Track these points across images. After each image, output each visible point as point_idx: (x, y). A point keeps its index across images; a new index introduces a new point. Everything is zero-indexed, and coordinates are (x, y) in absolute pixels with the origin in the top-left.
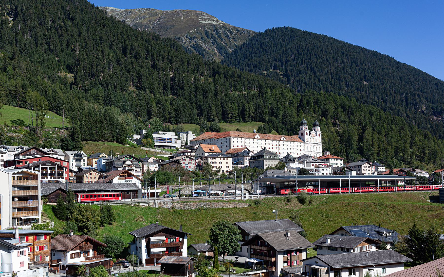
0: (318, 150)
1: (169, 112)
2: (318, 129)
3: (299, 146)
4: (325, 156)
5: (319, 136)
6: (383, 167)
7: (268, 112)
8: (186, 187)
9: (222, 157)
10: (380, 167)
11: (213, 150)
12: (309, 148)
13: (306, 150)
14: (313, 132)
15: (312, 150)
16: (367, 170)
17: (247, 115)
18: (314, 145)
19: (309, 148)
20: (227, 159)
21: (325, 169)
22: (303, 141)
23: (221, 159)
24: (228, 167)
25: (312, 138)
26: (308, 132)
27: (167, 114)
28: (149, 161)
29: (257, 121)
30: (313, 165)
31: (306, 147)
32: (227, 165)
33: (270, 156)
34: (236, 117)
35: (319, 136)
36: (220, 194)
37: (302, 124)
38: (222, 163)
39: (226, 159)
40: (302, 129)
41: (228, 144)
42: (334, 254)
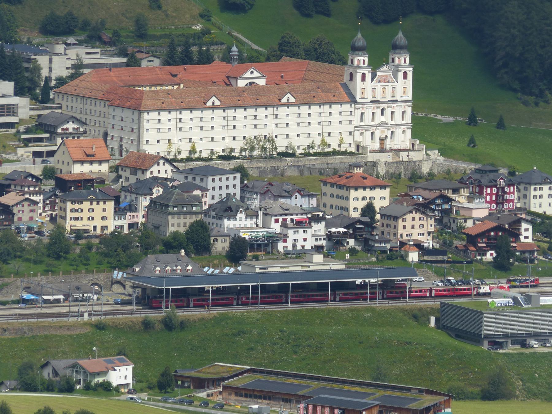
0: (398, 119)
8: (14, 281)
9: (94, 200)
11: (93, 156)
13: (358, 122)
15: (380, 119)
20: (105, 203)
22: (353, 100)
23: (91, 204)
24: (106, 218)
25: (379, 86)
30: (277, 221)
32: (104, 214)
36: (62, 300)
38: (93, 210)
41: (136, 127)
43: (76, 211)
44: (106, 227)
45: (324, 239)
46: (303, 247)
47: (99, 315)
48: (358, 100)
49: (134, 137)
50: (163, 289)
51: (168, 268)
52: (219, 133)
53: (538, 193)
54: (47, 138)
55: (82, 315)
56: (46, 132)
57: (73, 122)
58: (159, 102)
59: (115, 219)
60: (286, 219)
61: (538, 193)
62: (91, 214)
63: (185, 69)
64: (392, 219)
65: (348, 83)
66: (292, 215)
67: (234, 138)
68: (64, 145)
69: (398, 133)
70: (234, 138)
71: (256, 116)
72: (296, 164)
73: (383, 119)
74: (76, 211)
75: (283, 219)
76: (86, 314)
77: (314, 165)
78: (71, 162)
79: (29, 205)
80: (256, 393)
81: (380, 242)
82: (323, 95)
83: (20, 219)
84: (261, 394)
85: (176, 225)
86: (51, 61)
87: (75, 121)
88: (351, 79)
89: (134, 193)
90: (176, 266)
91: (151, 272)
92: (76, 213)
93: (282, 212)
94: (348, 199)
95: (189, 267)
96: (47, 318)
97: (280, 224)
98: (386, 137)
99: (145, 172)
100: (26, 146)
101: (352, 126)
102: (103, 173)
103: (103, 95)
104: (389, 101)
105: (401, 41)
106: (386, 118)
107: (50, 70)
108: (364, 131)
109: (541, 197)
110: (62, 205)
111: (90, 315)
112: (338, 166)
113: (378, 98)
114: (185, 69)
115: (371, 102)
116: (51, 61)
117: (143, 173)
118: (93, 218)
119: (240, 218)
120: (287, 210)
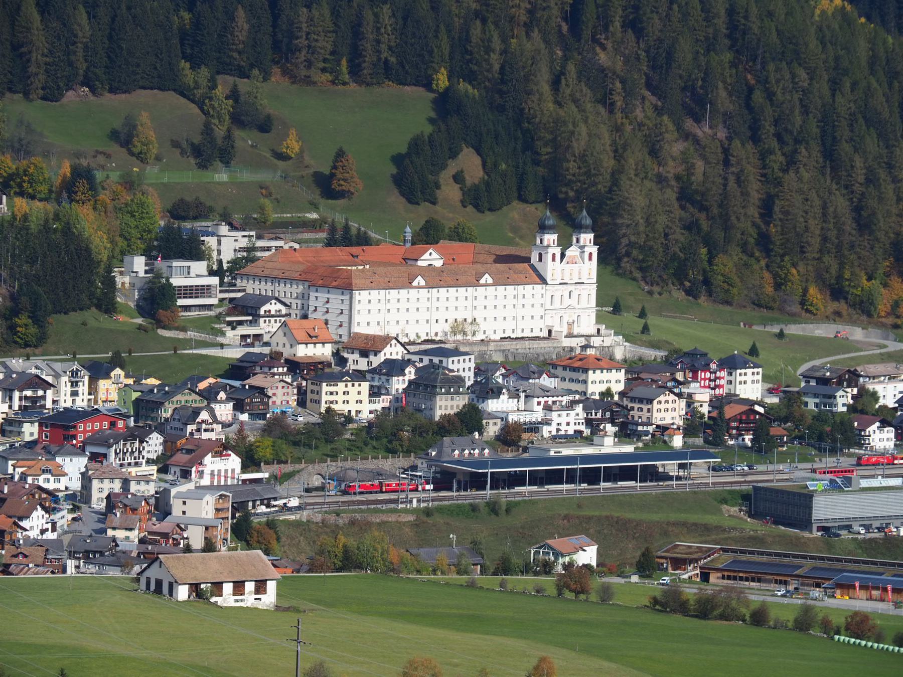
1: (86, 48)
3: (528, 296)
5: (590, 258)
6: (756, 370)
7: (446, 52)
9: (349, 381)
10: (743, 371)
11: (316, 337)
13: (548, 306)
14: (573, 252)
15: (567, 302)
16: (667, 410)
17: (369, 58)
19: (557, 299)
21: (564, 413)
22: (543, 281)
23: (346, 386)
26: (557, 251)
27: (80, 54)
28: (219, 398)
29: (405, 84)
30: (539, 403)
33: (450, 388)
34: (325, 60)
35: (590, 258)
39: (356, 384)
41: (345, 307)
42: (861, 609)
43: (331, 393)
44: (360, 411)
45: (583, 423)
46: (566, 431)
47: (428, 501)
48: (549, 282)
49: (344, 318)
50: (487, 472)
51: (467, 452)
52: (423, 315)
53: (743, 378)
54: (251, 321)
55: (411, 502)
56: (248, 315)
58: (368, 282)
61: (743, 378)
62: (346, 397)
63: (363, 250)
64: (645, 402)
65: (538, 266)
68: (285, 326)
69: (584, 318)
71: (457, 298)
72: (498, 348)
73: (569, 302)
74: (331, 393)
76: (415, 501)
77: (517, 349)
79: (283, 387)
80: (741, 575)
81: (643, 424)
82: (516, 276)
83: (274, 402)
84: (747, 575)
85: (443, 408)
86: (219, 243)
88: (540, 260)
89: (384, 374)
90: (474, 450)
91: (449, 456)
93: (543, 394)
94: (585, 382)
95: (487, 451)
96: (377, 504)
97: (541, 407)
100: (233, 328)
101: (543, 309)
102: (326, 357)
104: (576, 283)
106: (573, 301)
107: (219, 252)
108: (554, 315)
109: (745, 382)
110: (315, 388)
111: (418, 501)
112: (539, 351)
114: (363, 250)
115: (561, 284)
116: (219, 243)
118: (348, 402)
119: (503, 400)
120: (548, 391)
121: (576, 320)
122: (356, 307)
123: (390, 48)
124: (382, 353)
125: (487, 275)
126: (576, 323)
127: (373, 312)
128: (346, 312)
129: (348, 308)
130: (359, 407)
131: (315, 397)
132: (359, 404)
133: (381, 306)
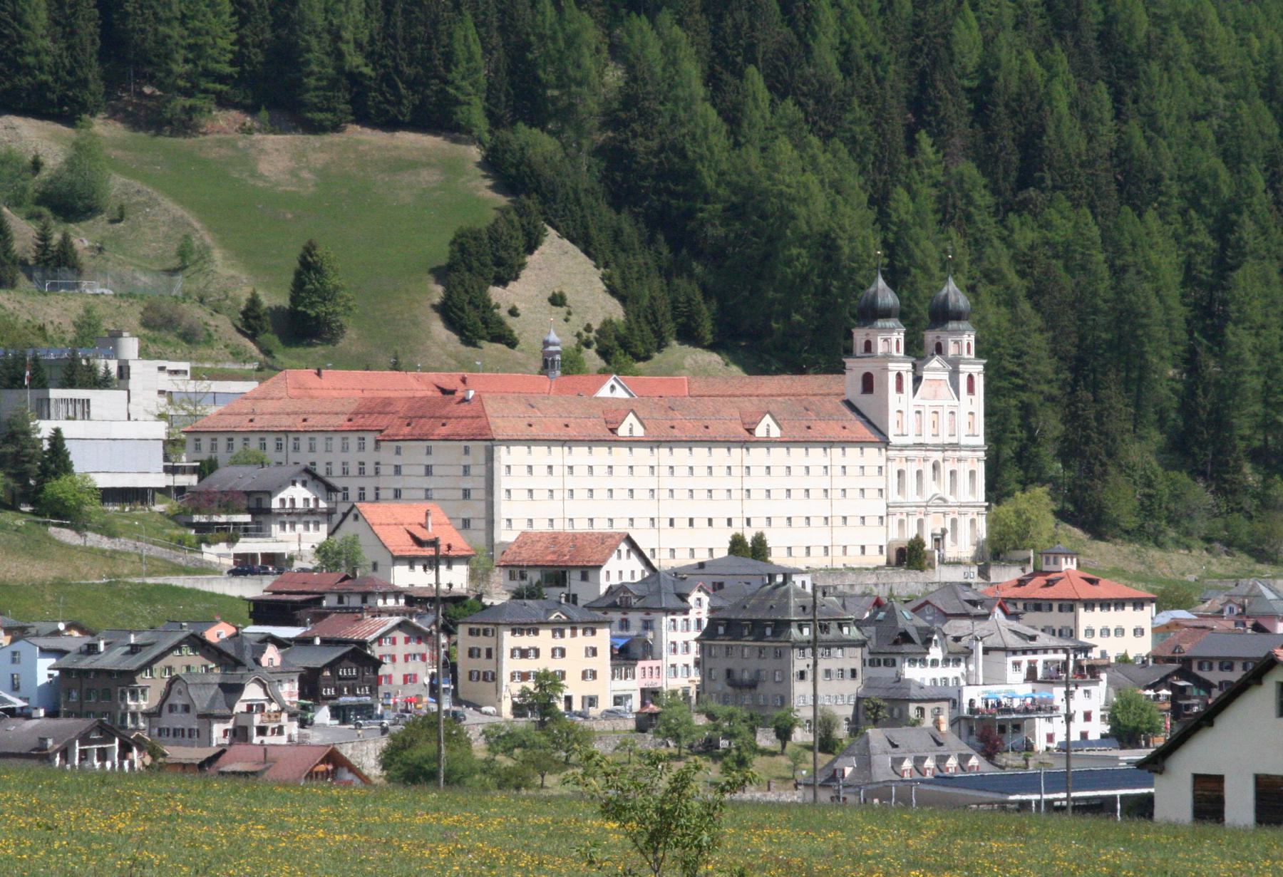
2: (963, 341)
4: (1050, 583)
5: (971, 389)
12: (911, 479)
14: (935, 370)
15: (931, 488)
18: (938, 456)
19: (911, 479)
22: (884, 442)
24: (594, 674)
26: (906, 367)
30: (1017, 665)
31: (893, 468)
35: (971, 389)
37: (871, 314)
40: (868, 346)
41: (476, 483)
43: (524, 654)
48: (893, 439)
57: (304, 484)
58: (522, 425)
59: (613, 677)
60: (1035, 662)
65: (862, 401)
66: (1045, 650)
67: (672, 522)
68: (356, 517)
70: (672, 522)
74: (524, 654)
75: (1030, 662)
78: (383, 559)
79: (407, 641)
87: (310, 483)
92: (524, 660)
98: (944, 532)
99: (591, 574)
101: (883, 503)
103: (350, 420)
105: (957, 301)
113: (928, 439)
117: (584, 577)
121: (948, 527)
122: (503, 481)
123: (359, 45)
124: (603, 572)
125: (768, 416)
126: (948, 536)
127: (540, 495)
128: (477, 494)
129: (482, 483)
130: (589, 688)
131: (482, 664)
132: (590, 682)
133: (554, 482)
